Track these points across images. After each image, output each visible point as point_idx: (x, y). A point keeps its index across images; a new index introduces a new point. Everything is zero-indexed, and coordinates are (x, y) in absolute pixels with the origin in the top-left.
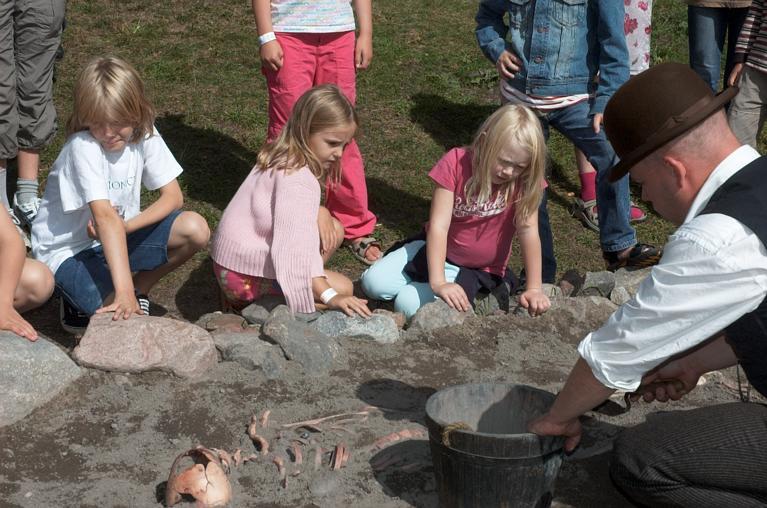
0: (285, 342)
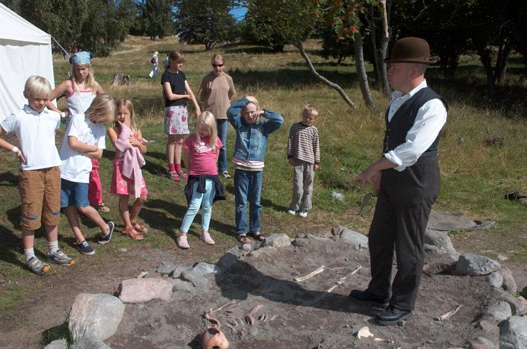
0: (193, 280)
